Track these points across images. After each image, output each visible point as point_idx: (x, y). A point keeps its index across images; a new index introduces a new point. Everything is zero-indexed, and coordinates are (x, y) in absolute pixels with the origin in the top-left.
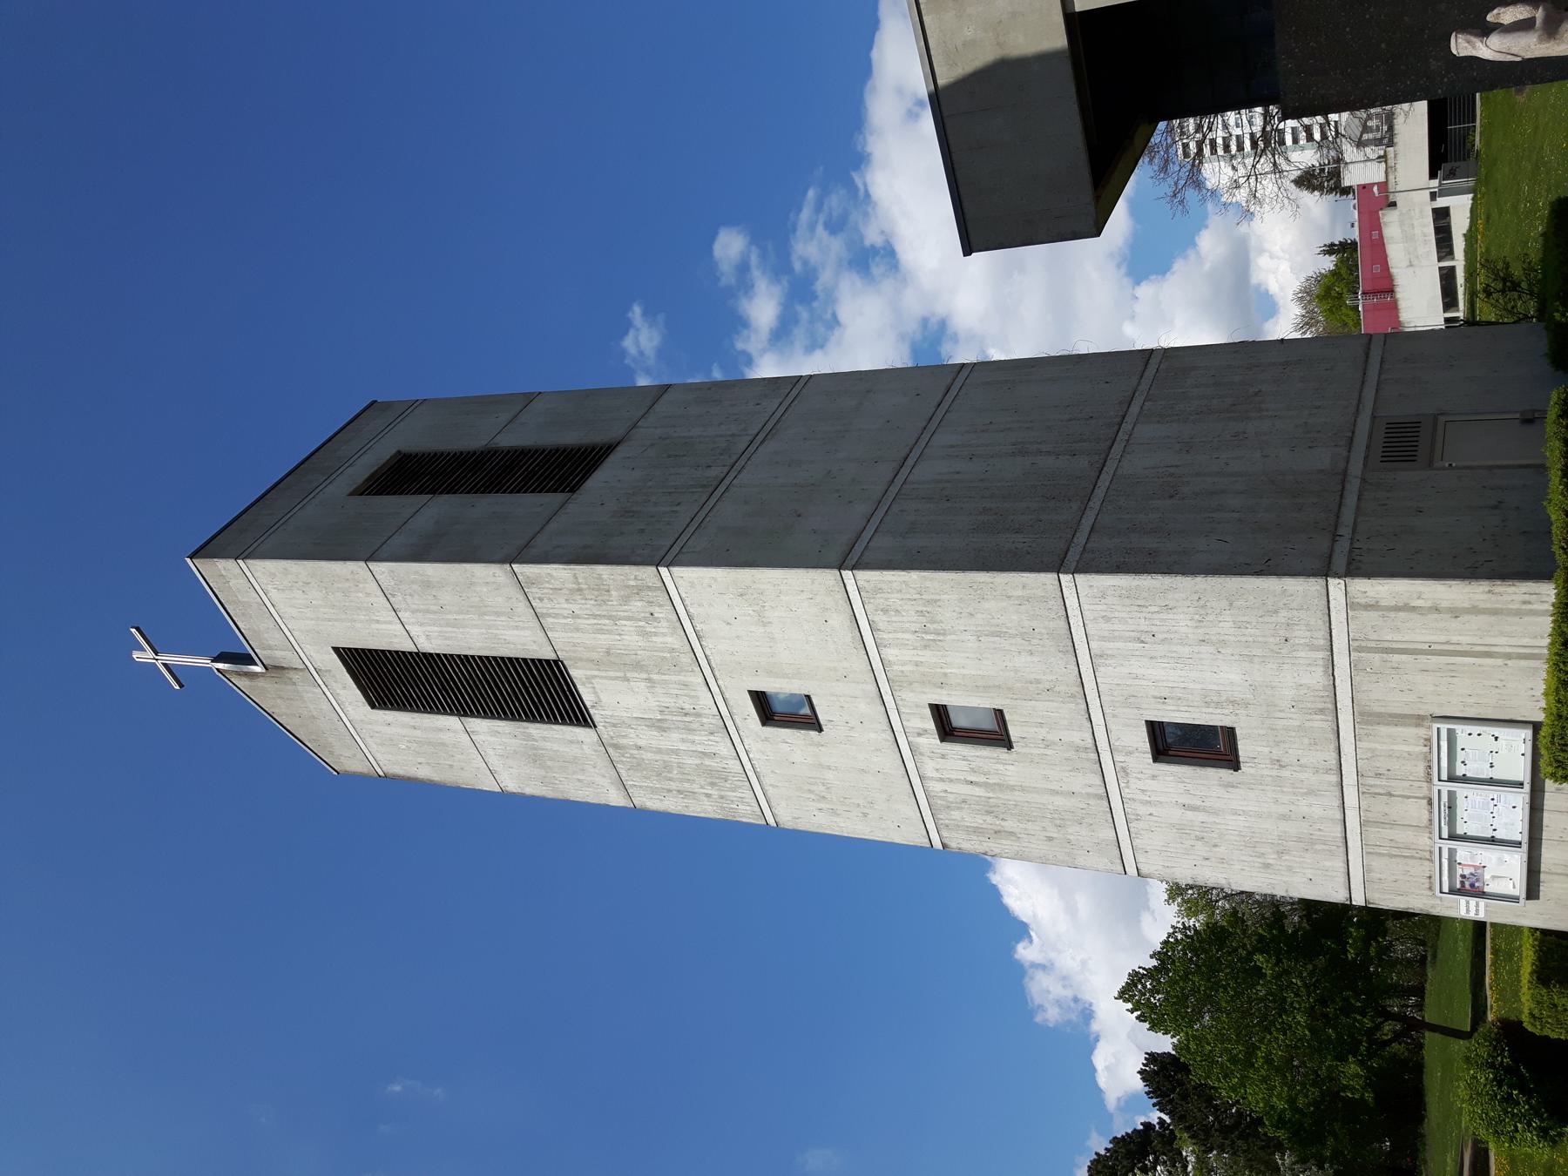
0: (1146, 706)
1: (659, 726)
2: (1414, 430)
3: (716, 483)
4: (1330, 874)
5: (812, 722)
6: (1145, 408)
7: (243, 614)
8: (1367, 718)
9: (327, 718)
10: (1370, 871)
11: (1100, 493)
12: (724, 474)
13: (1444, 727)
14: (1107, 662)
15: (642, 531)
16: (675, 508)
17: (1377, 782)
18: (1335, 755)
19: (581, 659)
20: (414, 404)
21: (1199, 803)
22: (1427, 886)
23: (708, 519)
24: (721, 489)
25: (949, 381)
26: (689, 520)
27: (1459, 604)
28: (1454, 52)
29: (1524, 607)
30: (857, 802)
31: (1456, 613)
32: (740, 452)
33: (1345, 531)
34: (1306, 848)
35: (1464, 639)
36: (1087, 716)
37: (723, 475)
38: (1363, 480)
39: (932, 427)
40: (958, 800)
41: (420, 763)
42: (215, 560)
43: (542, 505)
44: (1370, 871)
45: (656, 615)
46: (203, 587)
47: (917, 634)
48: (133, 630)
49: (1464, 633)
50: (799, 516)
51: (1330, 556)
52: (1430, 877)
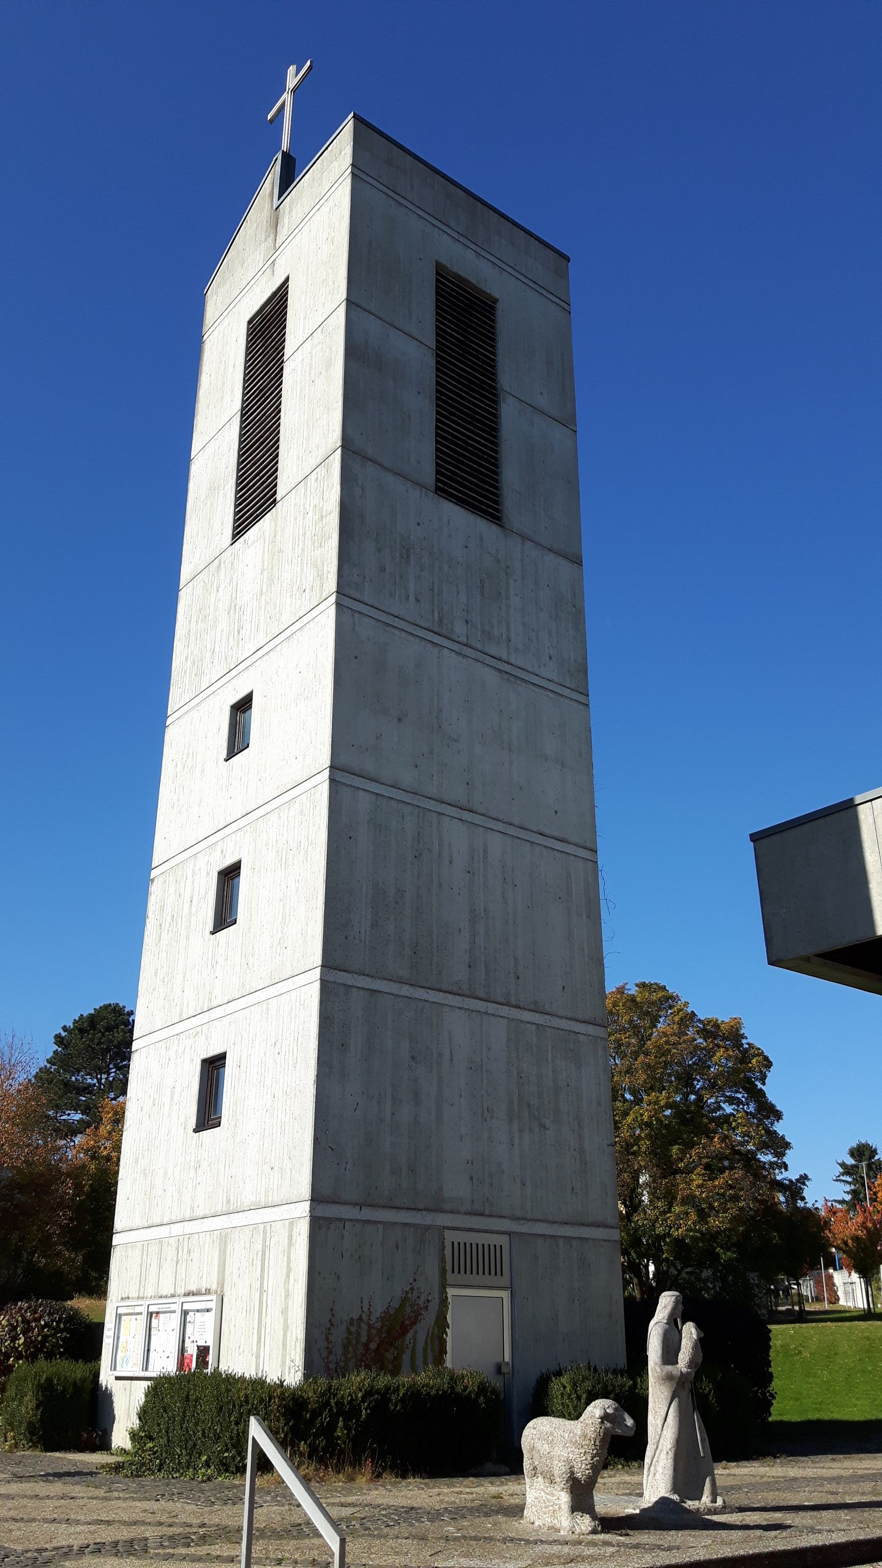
0: (235, 1050)
1: (232, 607)
2: (468, 1267)
3: (445, 632)
4: (131, 1214)
5: (232, 752)
6: (529, 1025)
7: (314, 179)
8: (224, 1239)
9: (242, 277)
10: (132, 1247)
11: (420, 993)
12: (457, 639)
13: (212, 1305)
14: (264, 1014)
15: (382, 569)
16: (412, 598)
17: (185, 1251)
18: (201, 1214)
19: (276, 525)
20: (564, 307)
21: (175, 1101)
22: (124, 1296)
23: (397, 632)
24: (437, 639)
25: (572, 839)
26: (396, 614)
27: (290, 1314)
28: (663, 1294)
29: (287, 1368)
30: (181, 800)
31: (285, 1311)
32: (486, 650)
33: (367, 1214)
34: (147, 1193)
35: (268, 1320)
36: (231, 1000)
37: (455, 637)
38: (428, 1228)
39: (511, 831)
40: (181, 890)
41: (210, 375)
42: (352, 144)
43: (419, 463)
44: (132, 1247)
45: (304, 595)
46: (333, 133)
47: (286, 843)
48: (308, 63)
49: (273, 1320)
50: (400, 720)
51: (335, 1202)
52: (128, 1298)
